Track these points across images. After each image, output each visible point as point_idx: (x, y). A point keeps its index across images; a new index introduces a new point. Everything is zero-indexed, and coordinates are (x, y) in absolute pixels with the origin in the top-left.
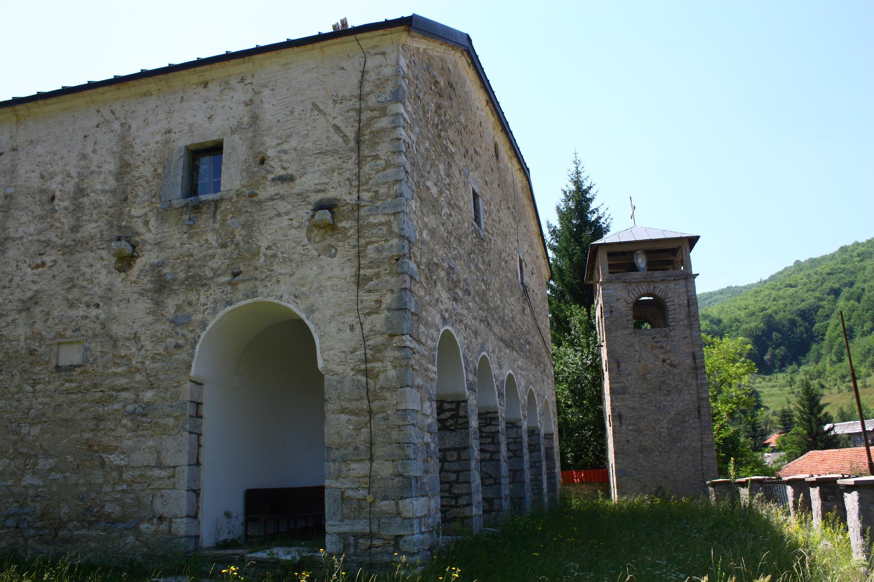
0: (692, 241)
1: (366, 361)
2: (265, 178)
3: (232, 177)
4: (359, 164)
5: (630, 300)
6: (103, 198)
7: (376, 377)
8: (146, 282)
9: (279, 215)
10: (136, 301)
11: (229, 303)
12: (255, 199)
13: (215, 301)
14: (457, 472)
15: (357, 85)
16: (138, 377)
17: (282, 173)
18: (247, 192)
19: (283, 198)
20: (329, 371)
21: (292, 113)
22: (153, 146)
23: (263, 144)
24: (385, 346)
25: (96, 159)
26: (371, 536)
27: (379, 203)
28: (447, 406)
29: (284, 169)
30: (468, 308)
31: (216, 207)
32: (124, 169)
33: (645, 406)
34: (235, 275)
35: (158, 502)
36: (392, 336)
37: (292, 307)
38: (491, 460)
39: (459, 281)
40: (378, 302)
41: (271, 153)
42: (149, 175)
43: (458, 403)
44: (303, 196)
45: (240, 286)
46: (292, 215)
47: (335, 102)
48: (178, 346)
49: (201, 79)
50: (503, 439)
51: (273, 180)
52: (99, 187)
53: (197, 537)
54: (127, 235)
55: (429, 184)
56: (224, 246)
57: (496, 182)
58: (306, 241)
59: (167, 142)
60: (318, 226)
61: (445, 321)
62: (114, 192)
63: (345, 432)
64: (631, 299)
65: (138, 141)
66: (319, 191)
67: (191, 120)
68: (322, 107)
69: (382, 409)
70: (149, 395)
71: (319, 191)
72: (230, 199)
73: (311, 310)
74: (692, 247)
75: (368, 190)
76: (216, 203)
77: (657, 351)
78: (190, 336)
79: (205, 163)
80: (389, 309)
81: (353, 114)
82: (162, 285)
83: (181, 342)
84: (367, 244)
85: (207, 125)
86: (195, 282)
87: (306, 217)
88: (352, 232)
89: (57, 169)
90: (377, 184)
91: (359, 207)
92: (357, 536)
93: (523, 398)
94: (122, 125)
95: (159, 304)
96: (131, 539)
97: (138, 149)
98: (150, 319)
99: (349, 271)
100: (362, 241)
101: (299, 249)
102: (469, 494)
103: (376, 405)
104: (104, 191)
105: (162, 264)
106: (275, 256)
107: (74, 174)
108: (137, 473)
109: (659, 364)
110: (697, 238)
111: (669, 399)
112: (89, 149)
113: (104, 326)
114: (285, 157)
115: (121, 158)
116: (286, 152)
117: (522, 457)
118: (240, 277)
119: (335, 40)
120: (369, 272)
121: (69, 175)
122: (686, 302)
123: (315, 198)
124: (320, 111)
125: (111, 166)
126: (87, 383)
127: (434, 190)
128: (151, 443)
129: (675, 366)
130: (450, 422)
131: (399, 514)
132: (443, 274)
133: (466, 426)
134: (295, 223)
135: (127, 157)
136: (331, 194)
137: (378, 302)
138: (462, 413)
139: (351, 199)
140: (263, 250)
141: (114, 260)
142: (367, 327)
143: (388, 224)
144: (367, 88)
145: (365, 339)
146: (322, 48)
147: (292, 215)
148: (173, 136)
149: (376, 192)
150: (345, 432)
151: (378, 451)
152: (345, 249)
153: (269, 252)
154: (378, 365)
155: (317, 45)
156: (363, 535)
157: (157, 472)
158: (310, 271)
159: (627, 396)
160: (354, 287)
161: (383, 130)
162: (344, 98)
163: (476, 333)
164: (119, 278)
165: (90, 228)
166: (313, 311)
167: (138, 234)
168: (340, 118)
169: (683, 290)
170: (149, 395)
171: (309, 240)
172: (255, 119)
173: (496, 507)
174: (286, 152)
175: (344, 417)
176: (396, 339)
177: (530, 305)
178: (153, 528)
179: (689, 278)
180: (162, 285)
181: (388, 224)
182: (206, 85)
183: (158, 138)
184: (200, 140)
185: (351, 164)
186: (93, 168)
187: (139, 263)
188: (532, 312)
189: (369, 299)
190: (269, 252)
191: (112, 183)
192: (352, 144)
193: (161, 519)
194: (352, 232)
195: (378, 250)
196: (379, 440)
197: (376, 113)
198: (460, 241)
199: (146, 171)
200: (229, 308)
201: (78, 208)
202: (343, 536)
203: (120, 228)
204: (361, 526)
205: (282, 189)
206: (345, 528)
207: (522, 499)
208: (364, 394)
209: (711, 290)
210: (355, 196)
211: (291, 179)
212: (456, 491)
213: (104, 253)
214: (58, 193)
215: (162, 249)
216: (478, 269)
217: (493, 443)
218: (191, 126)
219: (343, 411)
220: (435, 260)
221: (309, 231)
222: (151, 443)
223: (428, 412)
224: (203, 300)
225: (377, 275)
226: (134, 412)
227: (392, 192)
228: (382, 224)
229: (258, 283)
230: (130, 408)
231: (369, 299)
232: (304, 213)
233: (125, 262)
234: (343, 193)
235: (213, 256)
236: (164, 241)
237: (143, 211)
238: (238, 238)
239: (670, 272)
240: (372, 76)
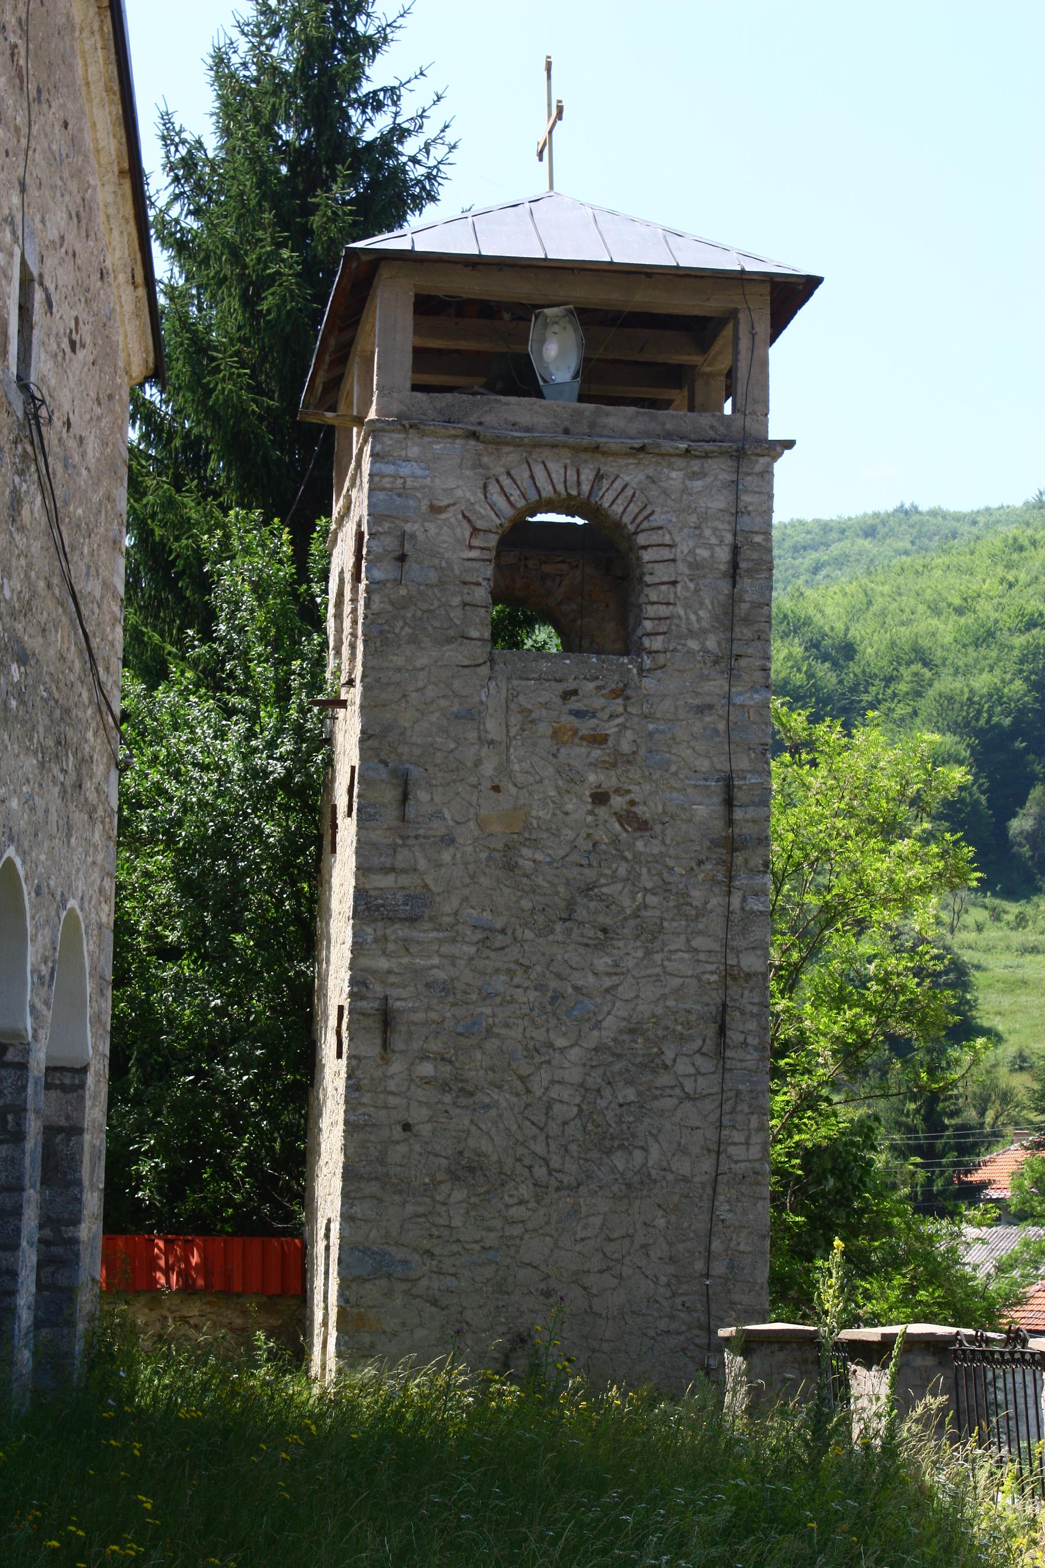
5: (486, 518)
33: (499, 983)
64: (495, 512)
74: (779, 322)
77: (578, 754)
109: (578, 807)
110: (810, 284)
111: (602, 962)
122: (723, 555)
129: (643, 826)
169: (719, 502)
179: (753, 452)
188: (54, 518)
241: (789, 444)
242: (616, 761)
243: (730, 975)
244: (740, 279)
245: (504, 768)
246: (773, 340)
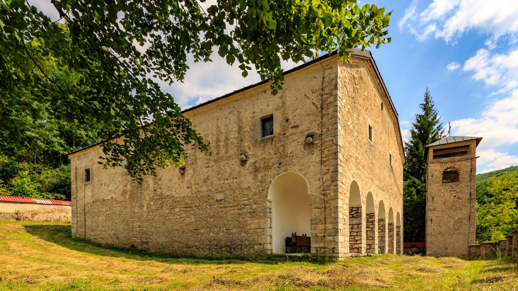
0: (478, 141)
1: (324, 191)
2: (288, 127)
3: (277, 128)
4: (322, 118)
5: (442, 171)
6: (234, 140)
7: (327, 196)
8: (251, 169)
9: (294, 141)
10: (248, 176)
11: (278, 174)
12: (285, 136)
13: (274, 174)
14: (357, 232)
15: (321, 84)
16: (251, 201)
17: (295, 124)
18: (282, 133)
19: (295, 134)
20: (311, 195)
21: (297, 99)
22: (249, 119)
23: (287, 114)
24: (330, 185)
25: (230, 126)
26: (325, 248)
27: (329, 133)
28: (354, 209)
29: (295, 123)
30: (364, 173)
31: (272, 140)
32: (240, 128)
33: (444, 216)
34: (280, 164)
35: (259, 239)
36: (333, 181)
37: (299, 173)
38: (371, 231)
39: (360, 162)
40: (328, 170)
41: (290, 117)
42: (249, 130)
43: (358, 208)
44: (302, 133)
45: (282, 168)
46: (299, 140)
47: (313, 93)
48: (263, 190)
49: (263, 90)
50: (376, 223)
51: (291, 127)
52: (232, 136)
53: (272, 250)
54: (244, 153)
55: (349, 123)
56: (276, 154)
57: (381, 121)
58: (303, 150)
59: (253, 117)
60: (307, 144)
61: (353, 177)
62: (238, 138)
63: (317, 215)
64: (442, 170)
65: (244, 118)
66: (308, 130)
67: (261, 107)
68: (308, 95)
69: (329, 207)
70: (254, 206)
71: (308, 130)
72: (277, 137)
73: (305, 175)
74: (477, 144)
75: (325, 128)
76: (272, 139)
77: (452, 192)
78: (266, 186)
79: (267, 125)
80: (332, 172)
81: (320, 97)
82: (256, 170)
83: (264, 188)
84: (325, 149)
85: (267, 109)
86: (267, 168)
87: (304, 140)
88: (319, 145)
89: (210, 132)
90: (328, 125)
91: (322, 135)
92: (320, 248)
93: (387, 210)
94: (238, 112)
95: (256, 176)
96: (252, 251)
97: (244, 121)
98: (253, 181)
99: (318, 159)
100: (323, 148)
101: (301, 153)
102: (361, 240)
103: (327, 205)
104: (234, 138)
105: (256, 162)
106: (293, 156)
107: (215, 133)
108: (253, 231)
109: (452, 198)
110: (481, 138)
111: (455, 213)
112: (228, 123)
113: (239, 185)
114: (295, 118)
115: (239, 125)
116: (295, 116)
117: (385, 232)
118: (282, 165)
119: (314, 64)
120: (325, 159)
121: (213, 134)
122: (470, 170)
123: (306, 133)
124: (307, 97)
125: (236, 129)
126: (236, 204)
127: (351, 126)
128: (256, 221)
129: (460, 199)
130: (355, 215)
131: (334, 241)
132: (353, 160)
133: (361, 216)
134: (300, 143)
135: (241, 124)
136: (312, 131)
137: (328, 170)
138: (359, 212)
139: (319, 132)
140: (289, 154)
141: (240, 162)
142: (324, 179)
143: (332, 140)
144: (325, 84)
145: (323, 183)
146: (307, 69)
147: (299, 140)
148: (256, 114)
149: (328, 128)
150: (317, 215)
151: (328, 220)
152: (317, 152)
153: (291, 155)
154: (328, 192)
155: (305, 68)
156: (323, 248)
157: (258, 230)
158: (305, 161)
159: (435, 212)
160: (320, 165)
161: (331, 102)
162: (316, 90)
163: (366, 183)
164: (242, 169)
165: (231, 152)
166: (306, 175)
167: (247, 152)
168: (315, 99)
169: (469, 164)
170: (254, 206)
171: (305, 149)
172: (284, 103)
173: (372, 247)
174: (295, 116)
175: (317, 210)
176: (334, 182)
177: (393, 174)
178: (258, 247)
179: (473, 159)
180: (256, 170)
181: (332, 140)
182: (265, 92)
183: (251, 115)
184: (264, 115)
185: (319, 118)
186: (230, 130)
187: (248, 163)
188: (394, 177)
189: (325, 169)
190: (291, 155)
191: (237, 135)
192: (320, 110)
193: (260, 244)
194: (319, 145)
195: (329, 151)
196: (328, 217)
197: (328, 95)
198: (361, 147)
199: (247, 129)
200: (278, 176)
201: (227, 145)
202: (316, 248)
203: (241, 151)
204: (322, 245)
205: (294, 130)
206: (317, 245)
207: (359, 208)
208: (323, 202)
209: (501, 169)
210: (320, 130)
211: (298, 126)
212: (356, 239)
213: (237, 160)
214: (211, 141)
215: (255, 157)
216: (369, 158)
217: (372, 224)
218: (261, 109)
219: (316, 208)
220: (350, 154)
221: (304, 146)
222: (256, 221)
223: (346, 208)
224: (270, 173)
225: (328, 160)
226: (250, 212)
227: (334, 128)
228: (330, 141)
229: (288, 166)
230: (249, 211)
231: (325, 169)
232: (302, 140)
233: (243, 162)
234: (316, 130)
235: (272, 158)
236: (256, 154)
237: (248, 144)
238: (280, 151)
239: (466, 156)
240: (327, 79)
241: (211, 61)
242: (457, 192)
243: (470, 212)
244: (472, 140)
245: (444, 195)
246: (476, 146)
